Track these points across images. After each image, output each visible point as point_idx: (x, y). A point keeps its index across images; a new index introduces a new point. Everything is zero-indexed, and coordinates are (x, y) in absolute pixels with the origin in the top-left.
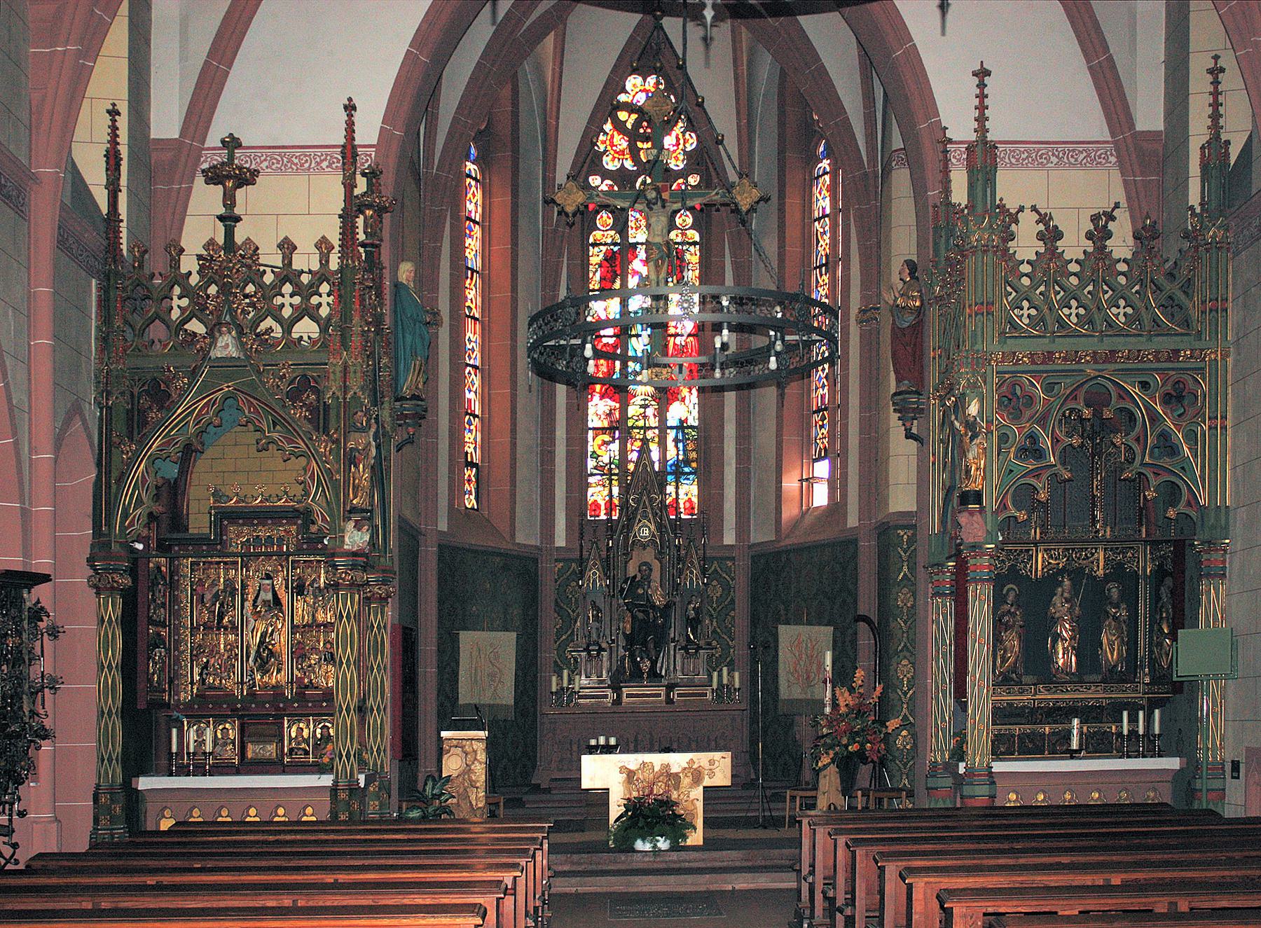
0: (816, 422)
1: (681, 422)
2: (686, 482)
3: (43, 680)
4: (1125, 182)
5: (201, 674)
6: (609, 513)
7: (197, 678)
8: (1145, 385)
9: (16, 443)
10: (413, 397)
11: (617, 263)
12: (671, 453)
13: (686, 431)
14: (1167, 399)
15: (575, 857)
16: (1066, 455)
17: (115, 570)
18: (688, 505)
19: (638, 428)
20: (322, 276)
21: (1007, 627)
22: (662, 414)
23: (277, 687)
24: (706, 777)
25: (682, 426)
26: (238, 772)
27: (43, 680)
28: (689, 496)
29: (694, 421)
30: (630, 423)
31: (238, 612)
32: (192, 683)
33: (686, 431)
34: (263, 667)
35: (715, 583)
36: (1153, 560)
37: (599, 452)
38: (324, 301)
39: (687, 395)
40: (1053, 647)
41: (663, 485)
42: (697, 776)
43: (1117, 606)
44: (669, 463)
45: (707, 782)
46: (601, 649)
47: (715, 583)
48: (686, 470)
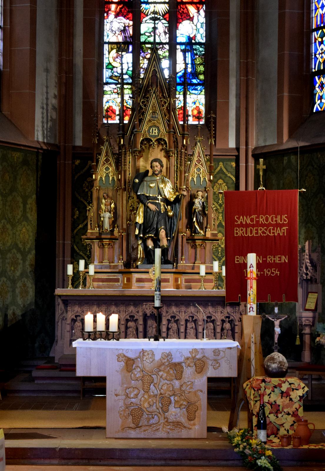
0: (316, 39)
1: (190, 39)
2: (194, 92)
3: (125, 311)
6: (121, 119)
12: (180, 67)
13: (194, 47)
18: (195, 112)
19: (149, 43)
22: (172, 30)
24: (211, 368)
25: (190, 43)
27: (125, 311)
28: (197, 104)
29: (201, 38)
30: (143, 39)
33: (194, 47)
35: (220, 181)
37: (114, 64)
39: (196, 15)
41: (172, 94)
44: (179, 75)
45: (211, 373)
47: (220, 181)
48: (194, 81)
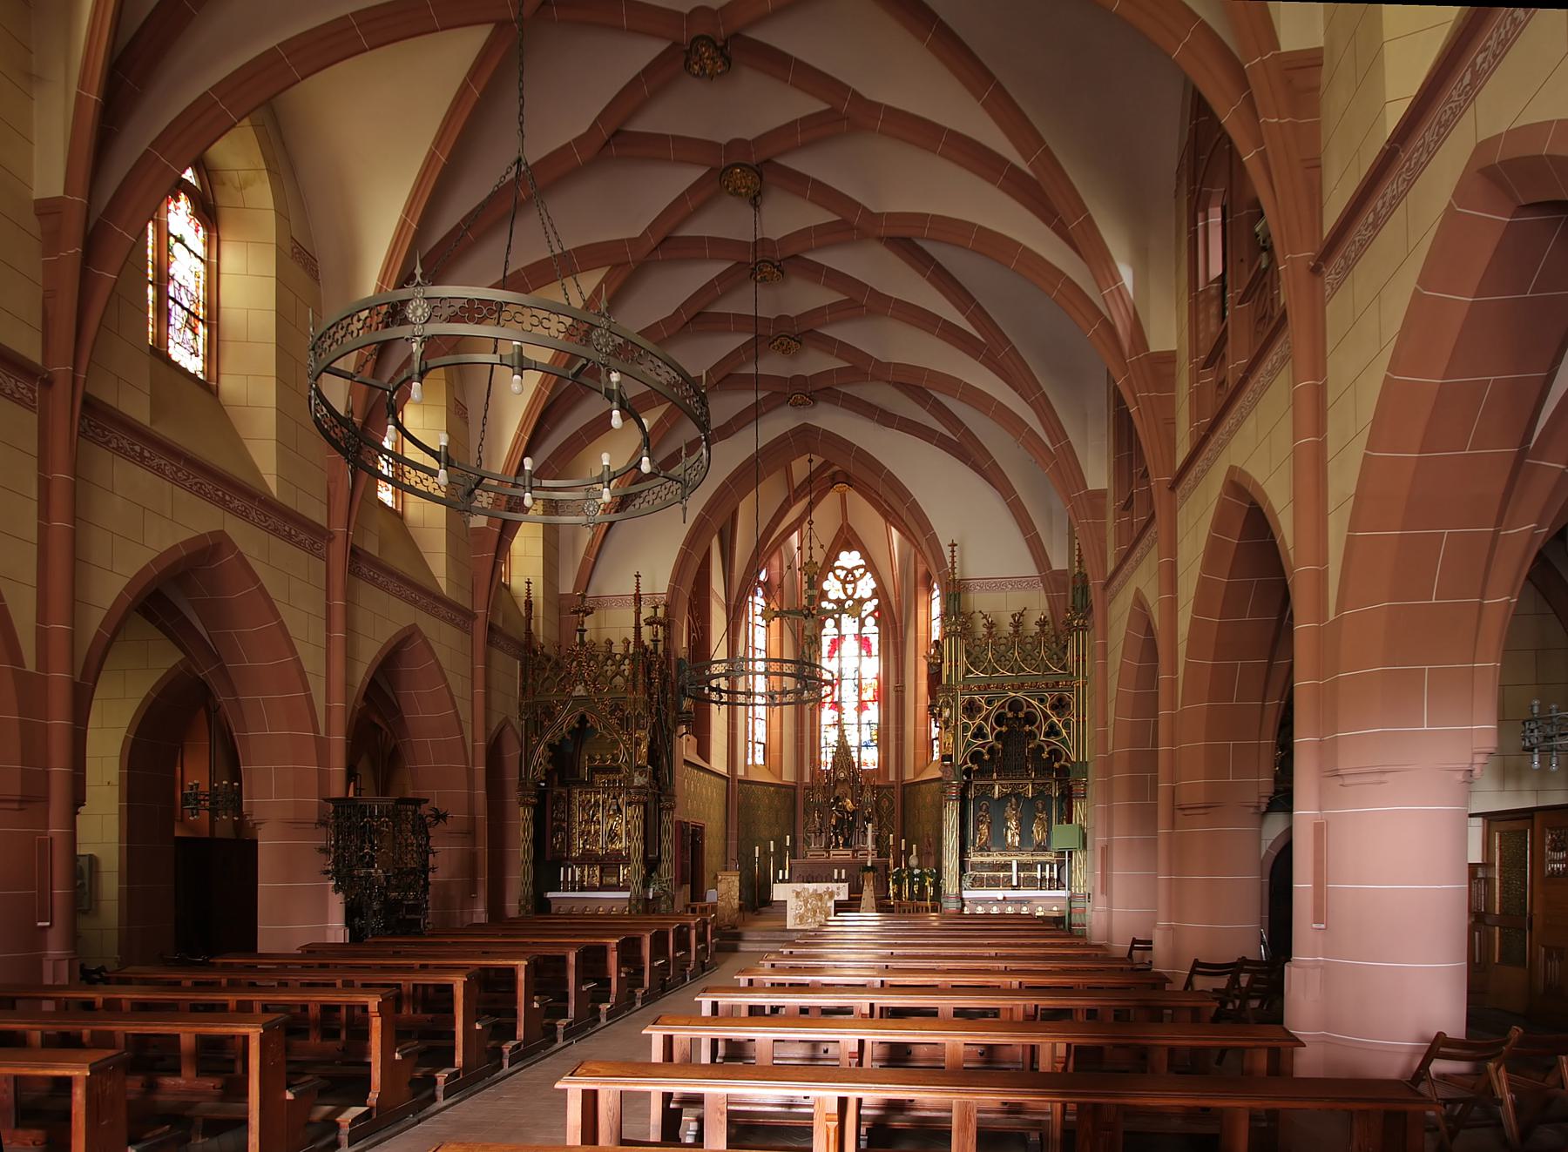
4: (1047, 596)
5: (583, 844)
7: (581, 846)
8: (1042, 701)
9: (463, 738)
10: (687, 712)
11: (836, 644)
14: (1053, 707)
15: (764, 934)
16: (998, 737)
17: (529, 795)
20: (624, 657)
21: (982, 823)
23: (619, 851)
26: (599, 890)
31: (601, 815)
32: (579, 848)
34: (612, 842)
36: (1059, 789)
38: (626, 667)
40: (1006, 833)
42: (831, 895)
43: (1042, 813)
45: (836, 898)
46: (821, 832)
